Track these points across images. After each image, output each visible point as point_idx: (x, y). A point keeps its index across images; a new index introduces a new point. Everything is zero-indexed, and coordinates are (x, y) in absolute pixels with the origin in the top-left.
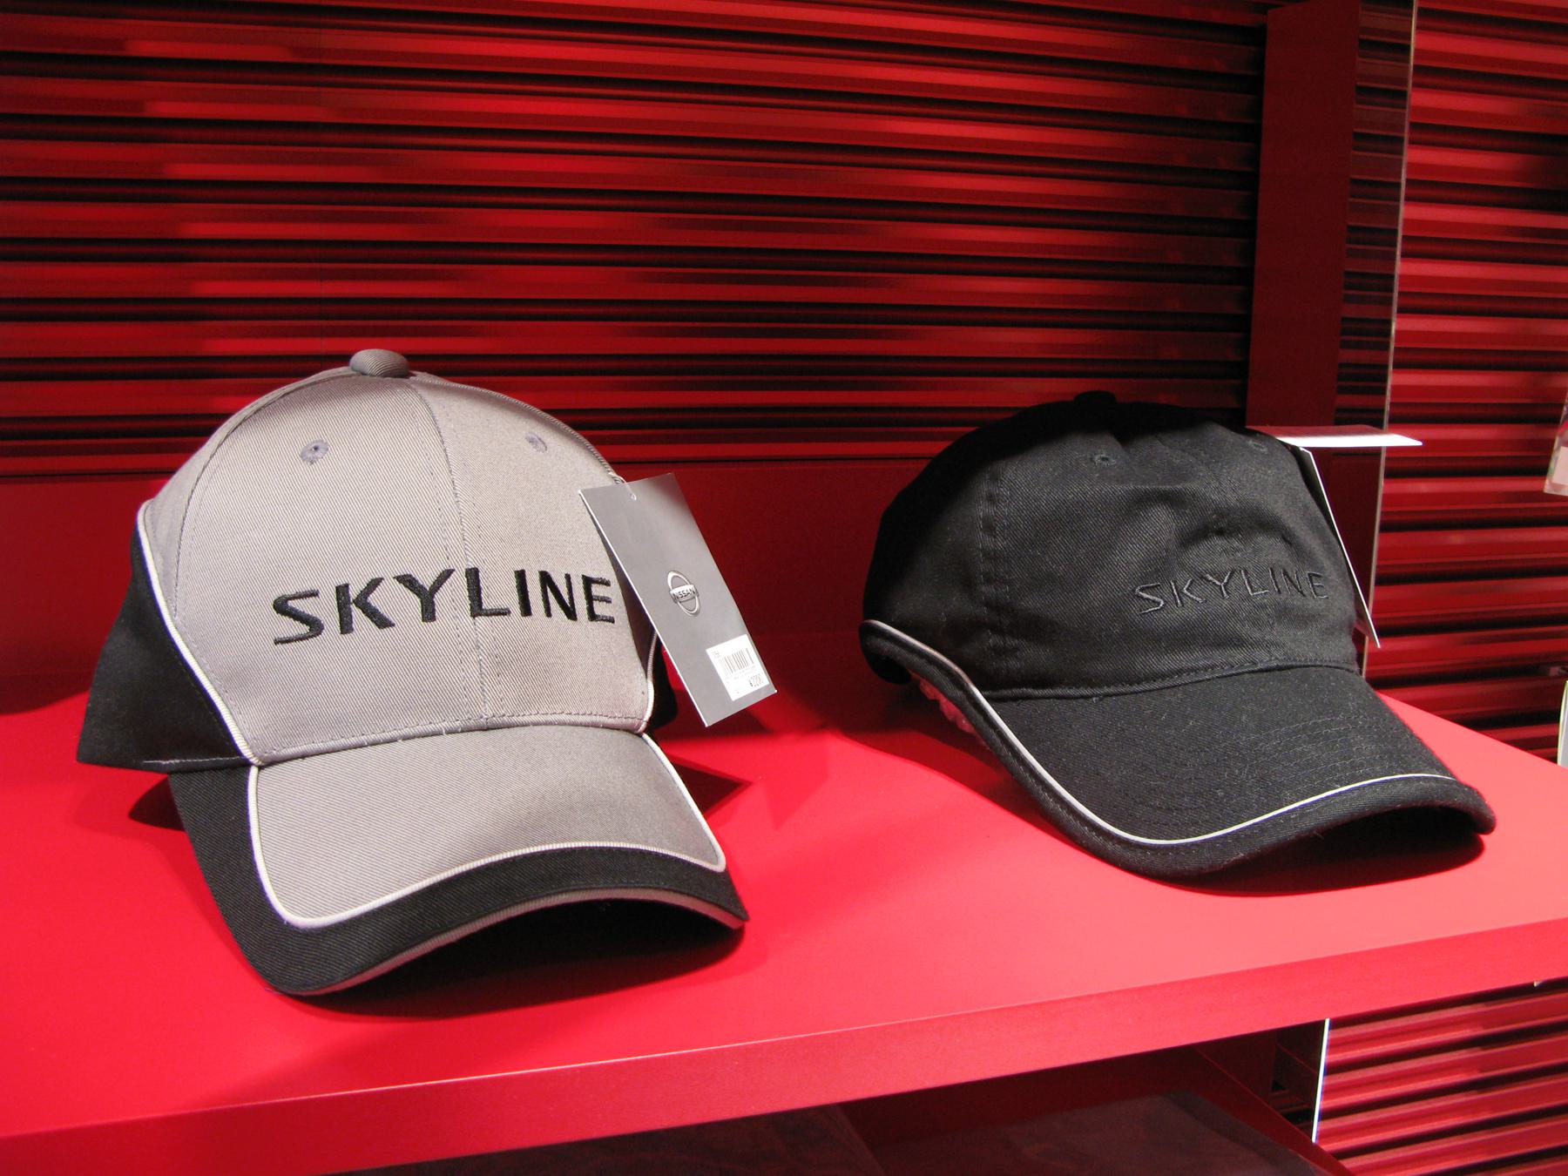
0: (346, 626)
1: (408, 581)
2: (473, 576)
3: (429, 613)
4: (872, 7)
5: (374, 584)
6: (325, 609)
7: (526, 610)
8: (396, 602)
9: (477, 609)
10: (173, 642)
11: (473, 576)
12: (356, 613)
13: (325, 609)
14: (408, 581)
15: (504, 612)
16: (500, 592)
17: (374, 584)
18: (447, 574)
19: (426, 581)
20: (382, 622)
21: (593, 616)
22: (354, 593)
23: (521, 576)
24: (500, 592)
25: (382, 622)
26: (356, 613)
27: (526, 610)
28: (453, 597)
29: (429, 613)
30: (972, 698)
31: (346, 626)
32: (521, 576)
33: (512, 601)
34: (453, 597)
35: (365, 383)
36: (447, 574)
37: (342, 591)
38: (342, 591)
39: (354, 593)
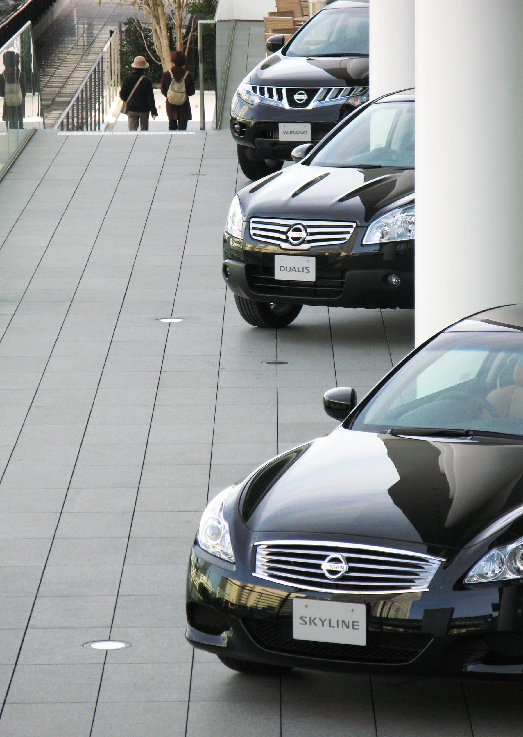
0: (310, 624)
1: (320, 619)
2: (330, 620)
3: (323, 625)
4: (371, 537)
5: (315, 619)
6: (307, 620)
7: (338, 626)
8: (317, 621)
9: (330, 626)
10: (276, 540)
11: (330, 620)
12: (312, 623)
13: (307, 620)
14: (320, 619)
15: (334, 627)
16: (334, 623)
17: (315, 619)
18: (326, 619)
19: (323, 620)
20: (315, 625)
21: (353, 628)
22: (312, 619)
23: (338, 621)
24: (334, 623)
25: (315, 625)
26: (312, 623)
27: (338, 626)
28: (327, 623)
29: (323, 625)
30: (29, 36)
31: (310, 624)
32: (338, 621)
33: (336, 625)
34: (327, 623)
35: (225, 279)
36: (326, 619)
37: (310, 618)
38: (310, 618)
39: (312, 619)
